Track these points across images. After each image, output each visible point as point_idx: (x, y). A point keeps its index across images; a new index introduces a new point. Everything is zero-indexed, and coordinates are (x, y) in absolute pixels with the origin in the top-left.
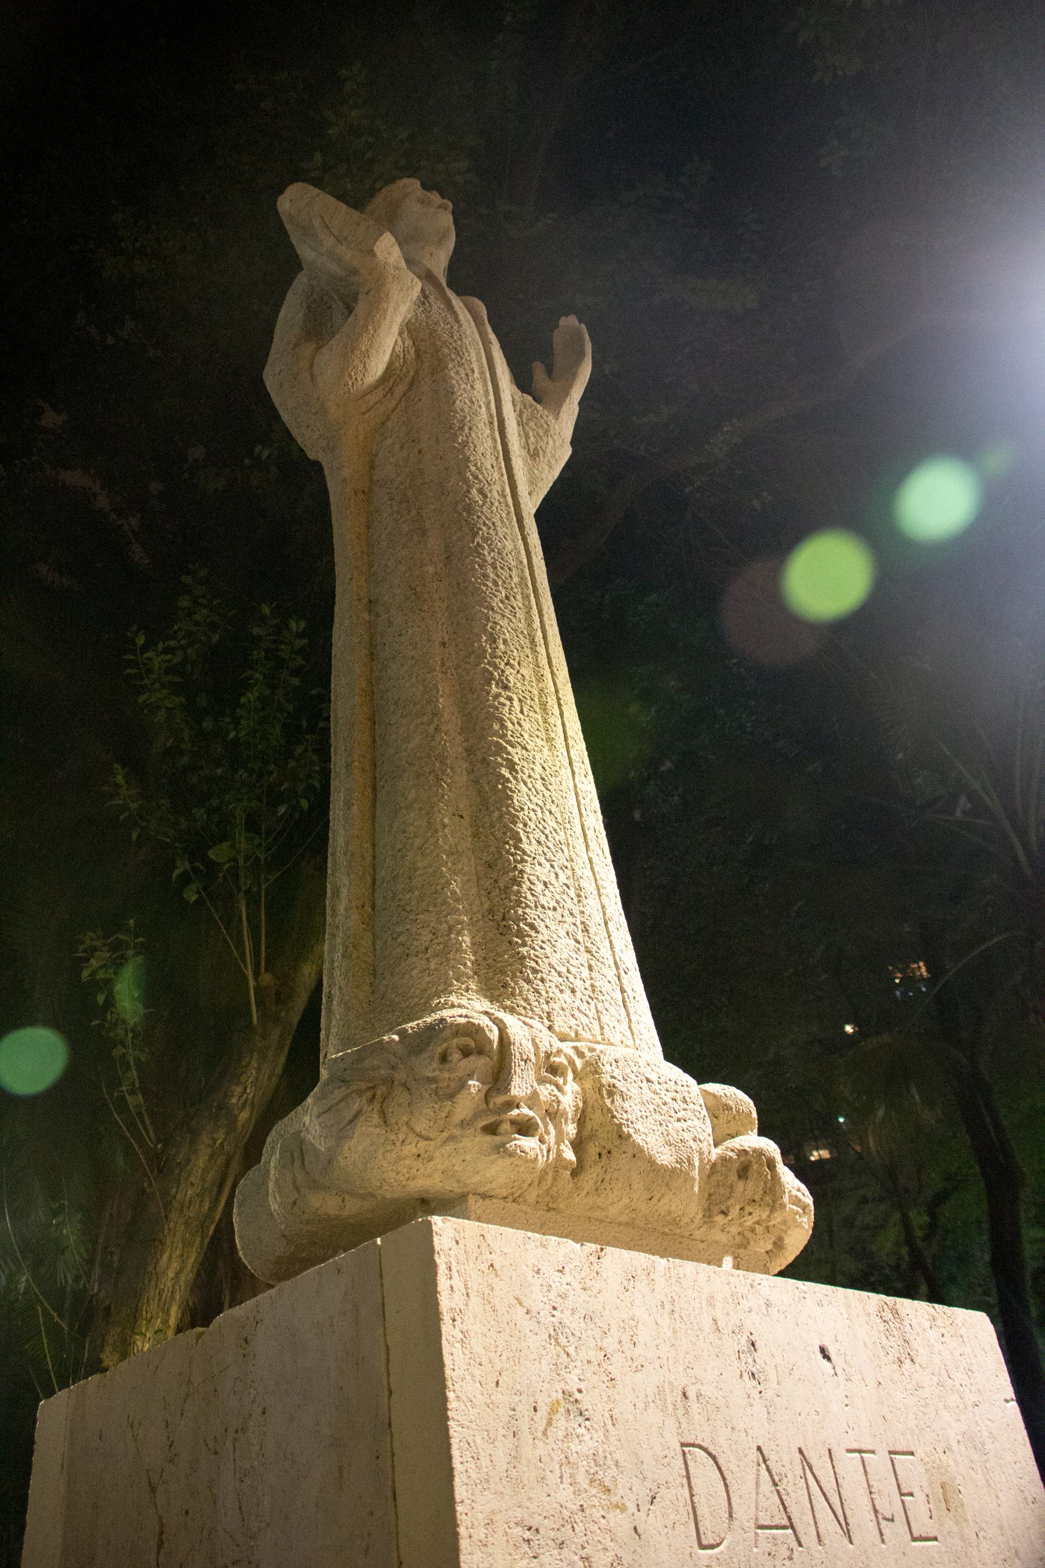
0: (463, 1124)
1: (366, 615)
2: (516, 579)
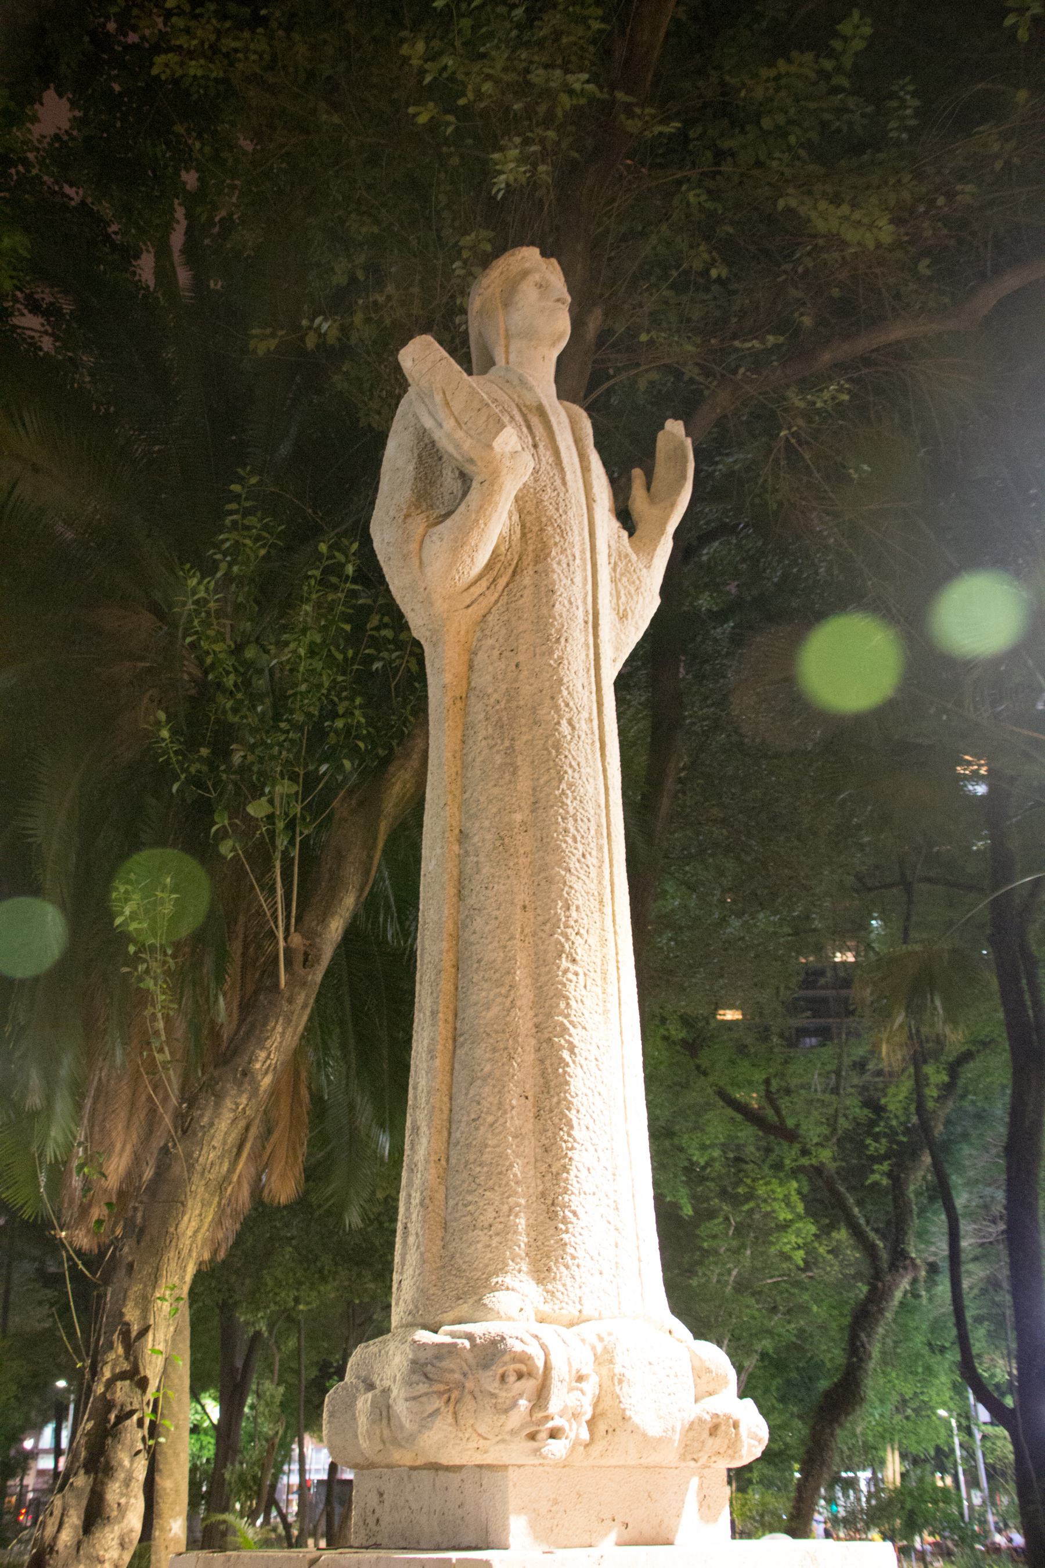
0: (513, 1432)
1: (456, 848)
2: (593, 832)
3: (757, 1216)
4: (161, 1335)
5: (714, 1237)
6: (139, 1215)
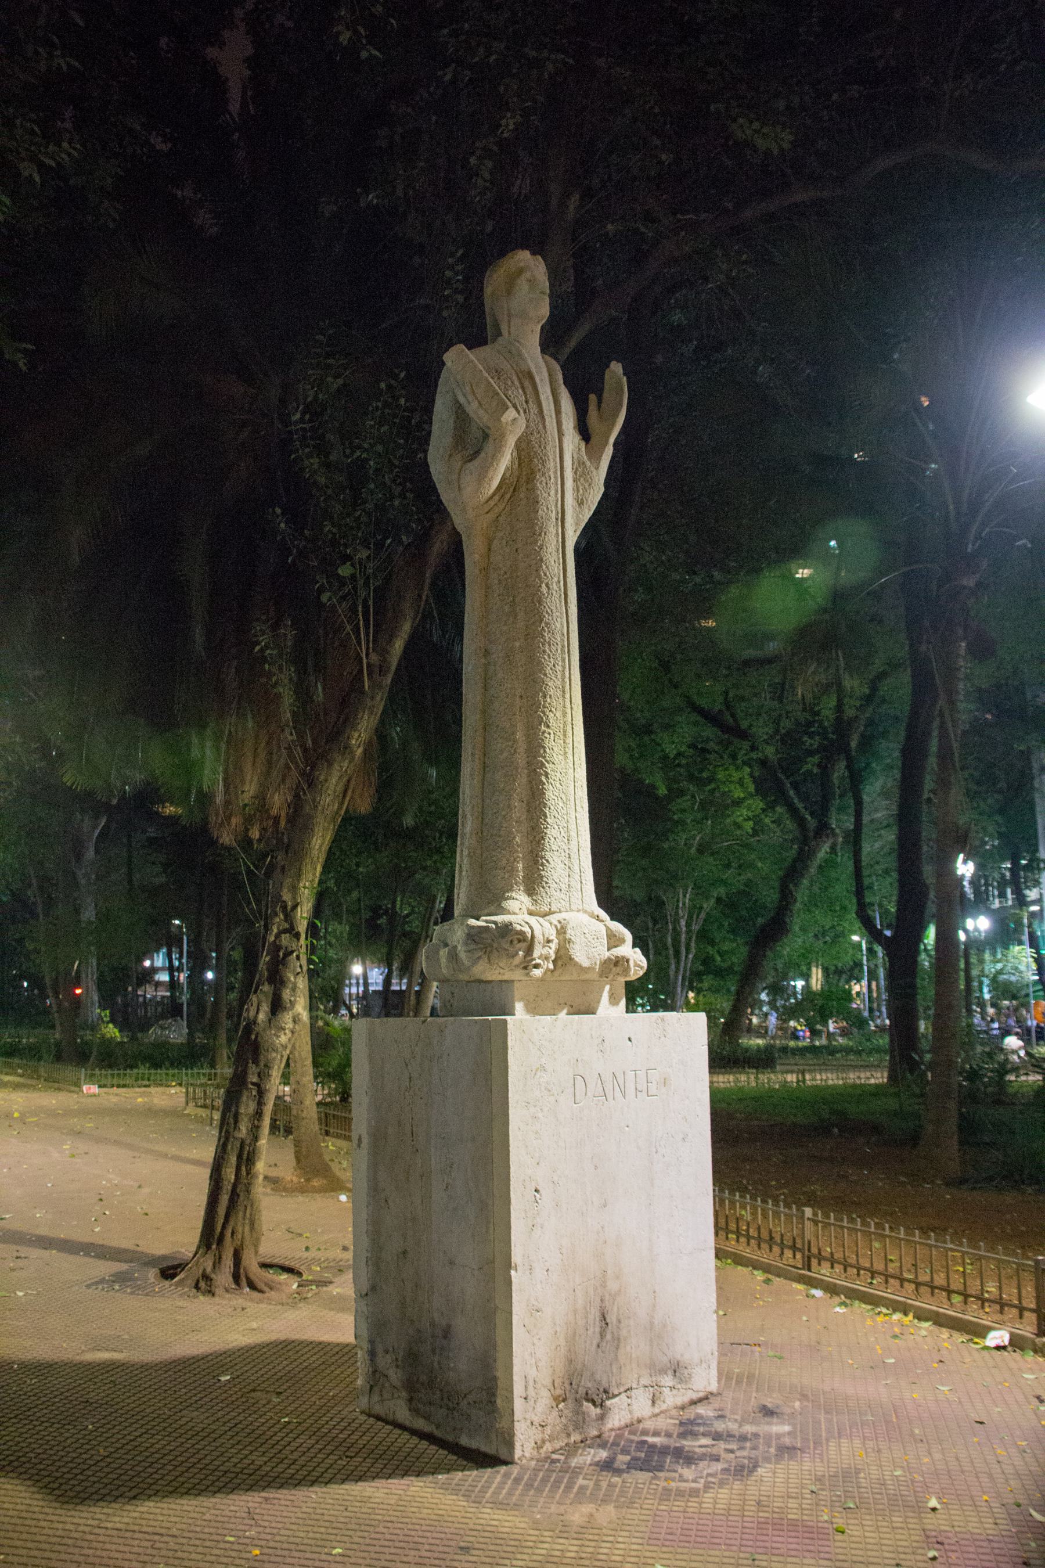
0: (516, 966)
3: (717, 794)
4: (305, 908)
5: (683, 811)
6: (285, 837)
